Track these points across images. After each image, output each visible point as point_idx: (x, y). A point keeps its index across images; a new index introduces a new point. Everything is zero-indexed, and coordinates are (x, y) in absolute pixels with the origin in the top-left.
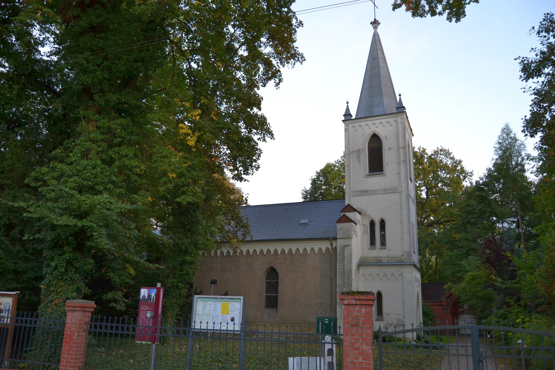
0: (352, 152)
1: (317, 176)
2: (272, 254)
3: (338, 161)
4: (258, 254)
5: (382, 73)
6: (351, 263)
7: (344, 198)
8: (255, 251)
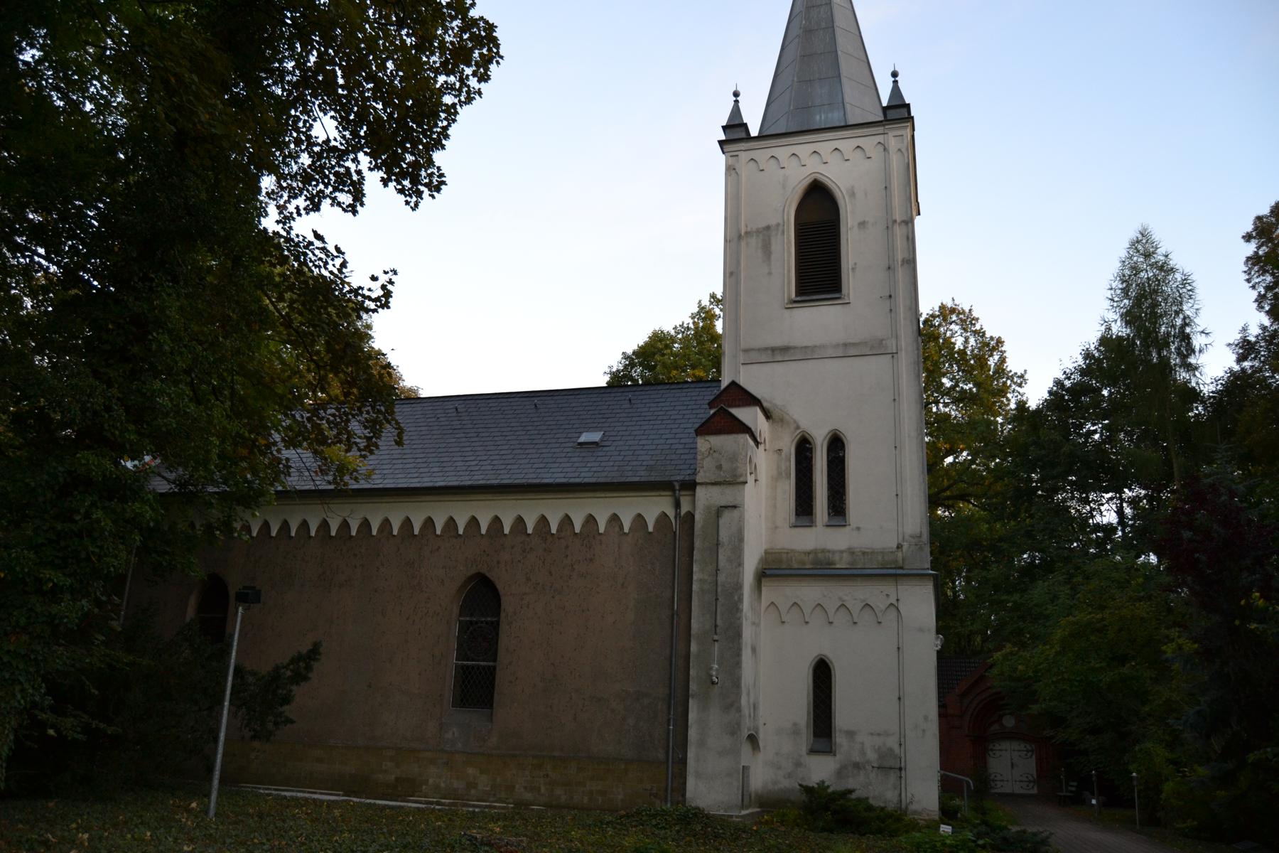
1: (626, 366)
2: (483, 531)
3: (682, 326)
4: (438, 532)
5: (840, 21)
6: (740, 564)
7: (717, 363)
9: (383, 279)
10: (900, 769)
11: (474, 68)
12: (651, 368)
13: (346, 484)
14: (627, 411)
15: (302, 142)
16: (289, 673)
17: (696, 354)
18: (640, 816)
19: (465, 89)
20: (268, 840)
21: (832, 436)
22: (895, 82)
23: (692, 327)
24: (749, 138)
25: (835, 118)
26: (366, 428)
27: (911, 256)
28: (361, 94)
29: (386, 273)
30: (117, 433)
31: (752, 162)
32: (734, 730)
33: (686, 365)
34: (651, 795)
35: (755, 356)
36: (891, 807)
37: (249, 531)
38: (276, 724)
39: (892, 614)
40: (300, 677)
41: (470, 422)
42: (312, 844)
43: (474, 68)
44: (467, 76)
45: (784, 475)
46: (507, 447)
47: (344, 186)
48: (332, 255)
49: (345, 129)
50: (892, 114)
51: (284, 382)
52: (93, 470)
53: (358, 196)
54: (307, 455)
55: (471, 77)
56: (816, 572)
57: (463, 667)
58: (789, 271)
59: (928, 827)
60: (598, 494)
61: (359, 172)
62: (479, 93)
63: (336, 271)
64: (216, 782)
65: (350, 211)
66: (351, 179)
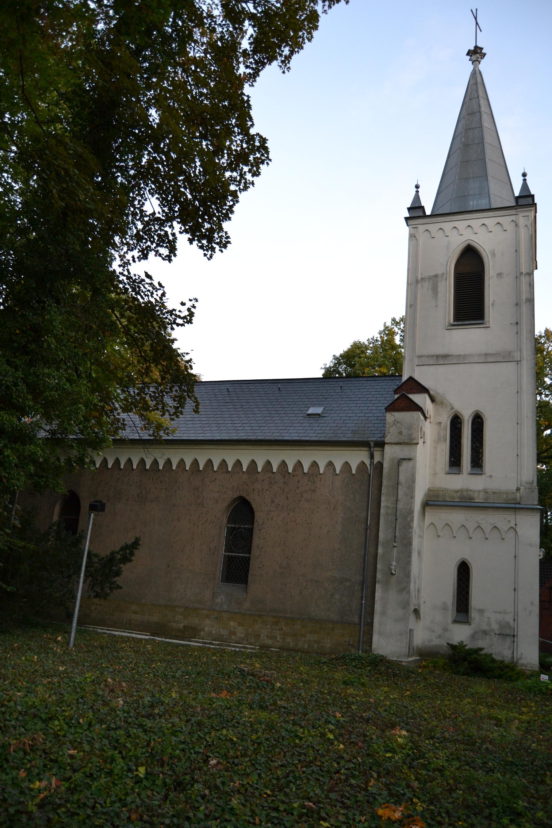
0: (422, 279)
3: (373, 339)
4: (215, 469)
5: (488, 138)
6: (413, 497)
8: (210, 462)
9: (189, 304)
10: (514, 636)
11: (250, 167)
12: (352, 366)
13: (161, 437)
14: (339, 394)
15: (137, 214)
16: (119, 556)
17: (382, 357)
18: (345, 660)
19: (243, 181)
20: (111, 665)
21: (454, 415)
22: (525, 180)
23: (380, 340)
24: (425, 216)
25: (483, 203)
26: (175, 401)
27: (532, 297)
28: (176, 183)
29: (191, 300)
30: (21, 400)
31: (427, 232)
32: (405, 605)
33: (375, 365)
34: (349, 644)
35: (425, 361)
36: (507, 660)
37: (94, 463)
38: (111, 589)
39: (512, 534)
40: (126, 559)
41: (236, 398)
42: (139, 669)
43: (250, 167)
44: (245, 172)
45: (442, 439)
46: (260, 415)
47: (163, 243)
48: (156, 288)
49: (165, 206)
50: (522, 202)
51: (123, 369)
52: (6, 424)
53: (173, 250)
54: (136, 418)
55: (247, 173)
56: (461, 504)
57: (228, 556)
58: (449, 305)
59: (532, 676)
60: (320, 448)
61: (173, 235)
62: (253, 183)
63: (158, 299)
64: (74, 624)
65: (167, 260)
66: (168, 239)
